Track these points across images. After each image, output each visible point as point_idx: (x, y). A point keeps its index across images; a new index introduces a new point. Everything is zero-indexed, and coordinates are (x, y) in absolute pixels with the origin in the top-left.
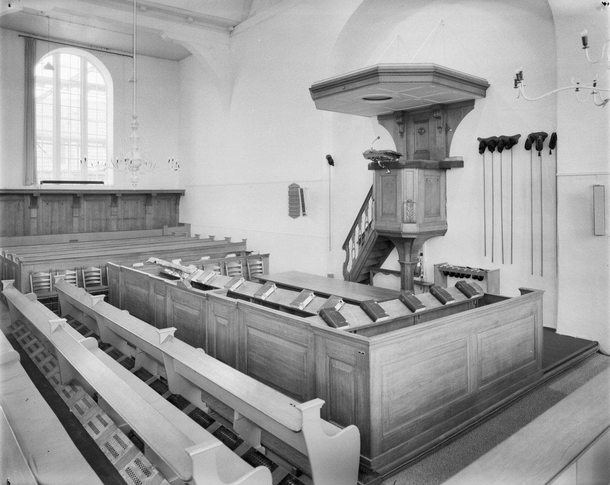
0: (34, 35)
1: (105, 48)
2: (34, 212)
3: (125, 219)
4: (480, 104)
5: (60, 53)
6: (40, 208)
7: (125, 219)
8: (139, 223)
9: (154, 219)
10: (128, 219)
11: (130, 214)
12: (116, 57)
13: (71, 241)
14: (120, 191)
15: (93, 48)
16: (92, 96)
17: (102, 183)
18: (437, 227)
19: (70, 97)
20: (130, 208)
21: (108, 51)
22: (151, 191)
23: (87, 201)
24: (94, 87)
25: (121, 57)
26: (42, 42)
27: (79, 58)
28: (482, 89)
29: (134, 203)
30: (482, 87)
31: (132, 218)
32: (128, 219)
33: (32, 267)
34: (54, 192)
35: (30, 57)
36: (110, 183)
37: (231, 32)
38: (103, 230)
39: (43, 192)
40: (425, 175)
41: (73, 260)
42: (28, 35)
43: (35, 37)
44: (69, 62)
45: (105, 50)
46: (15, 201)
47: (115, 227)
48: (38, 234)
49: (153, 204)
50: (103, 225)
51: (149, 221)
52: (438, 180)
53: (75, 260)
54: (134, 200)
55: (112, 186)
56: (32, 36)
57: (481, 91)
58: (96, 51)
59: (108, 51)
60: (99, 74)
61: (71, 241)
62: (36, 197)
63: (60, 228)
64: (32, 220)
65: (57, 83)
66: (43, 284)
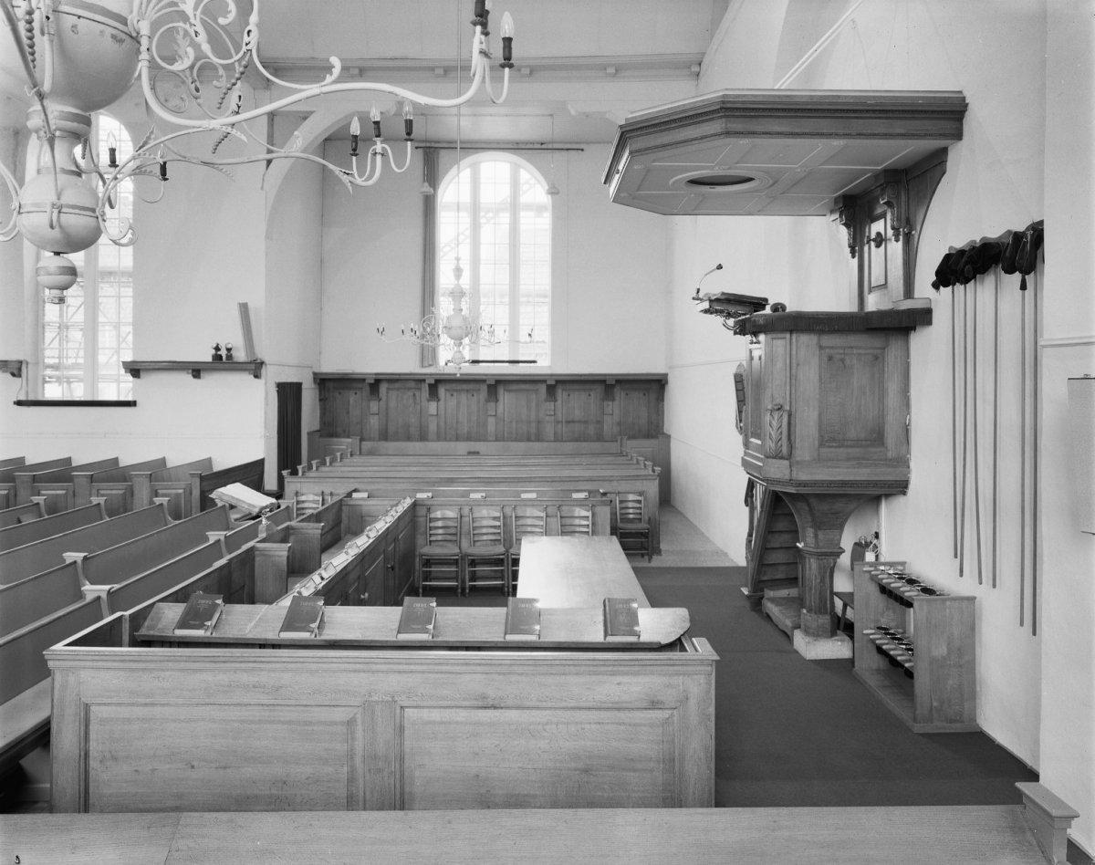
0: (436, 142)
1: (538, 143)
2: (374, 406)
3: (568, 422)
4: (960, 159)
5: (480, 162)
6: (559, 402)
7: (568, 422)
8: (591, 430)
9: (619, 424)
10: (573, 422)
11: (578, 414)
12: (557, 155)
13: (470, 453)
14: (612, 375)
15: (521, 146)
16: (526, 219)
17: (534, 362)
18: (868, 470)
19: (494, 234)
20: (576, 405)
21: (543, 146)
22: (486, 375)
23: (510, 391)
24: (529, 207)
25: (564, 153)
26: (446, 151)
27: (509, 165)
28: (949, 119)
29: (583, 396)
30: (947, 115)
31: (579, 422)
32: (573, 422)
33: (299, 485)
34: (586, 378)
35: (432, 175)
36: (545, 363)
37: (698, 75)
38: (533, 438)
39: (561, 378)
40: (821, 348)
41: (352, 480)
42: (428, 145)
43: (437, 145)
44: (495, 171)
45: (539, 146)
46: (409, 389)
47: (552, 435)
48: (439, 439)
49: (617, 398)
50: (533, 430)
51: (609, 426)
52: (876, 358)
53: (356, 480)
54: (584, 390)
55: (550, 367)
56: (433, 145)
57: (948, 126)
58: (530, 152)
59: (543, 146)
60: (535, 189)
61: (470, 453)
62: (612, 386)
63: (468, 433)
64: (430, 418)
65: (475, 208)
66: (577, 522)
